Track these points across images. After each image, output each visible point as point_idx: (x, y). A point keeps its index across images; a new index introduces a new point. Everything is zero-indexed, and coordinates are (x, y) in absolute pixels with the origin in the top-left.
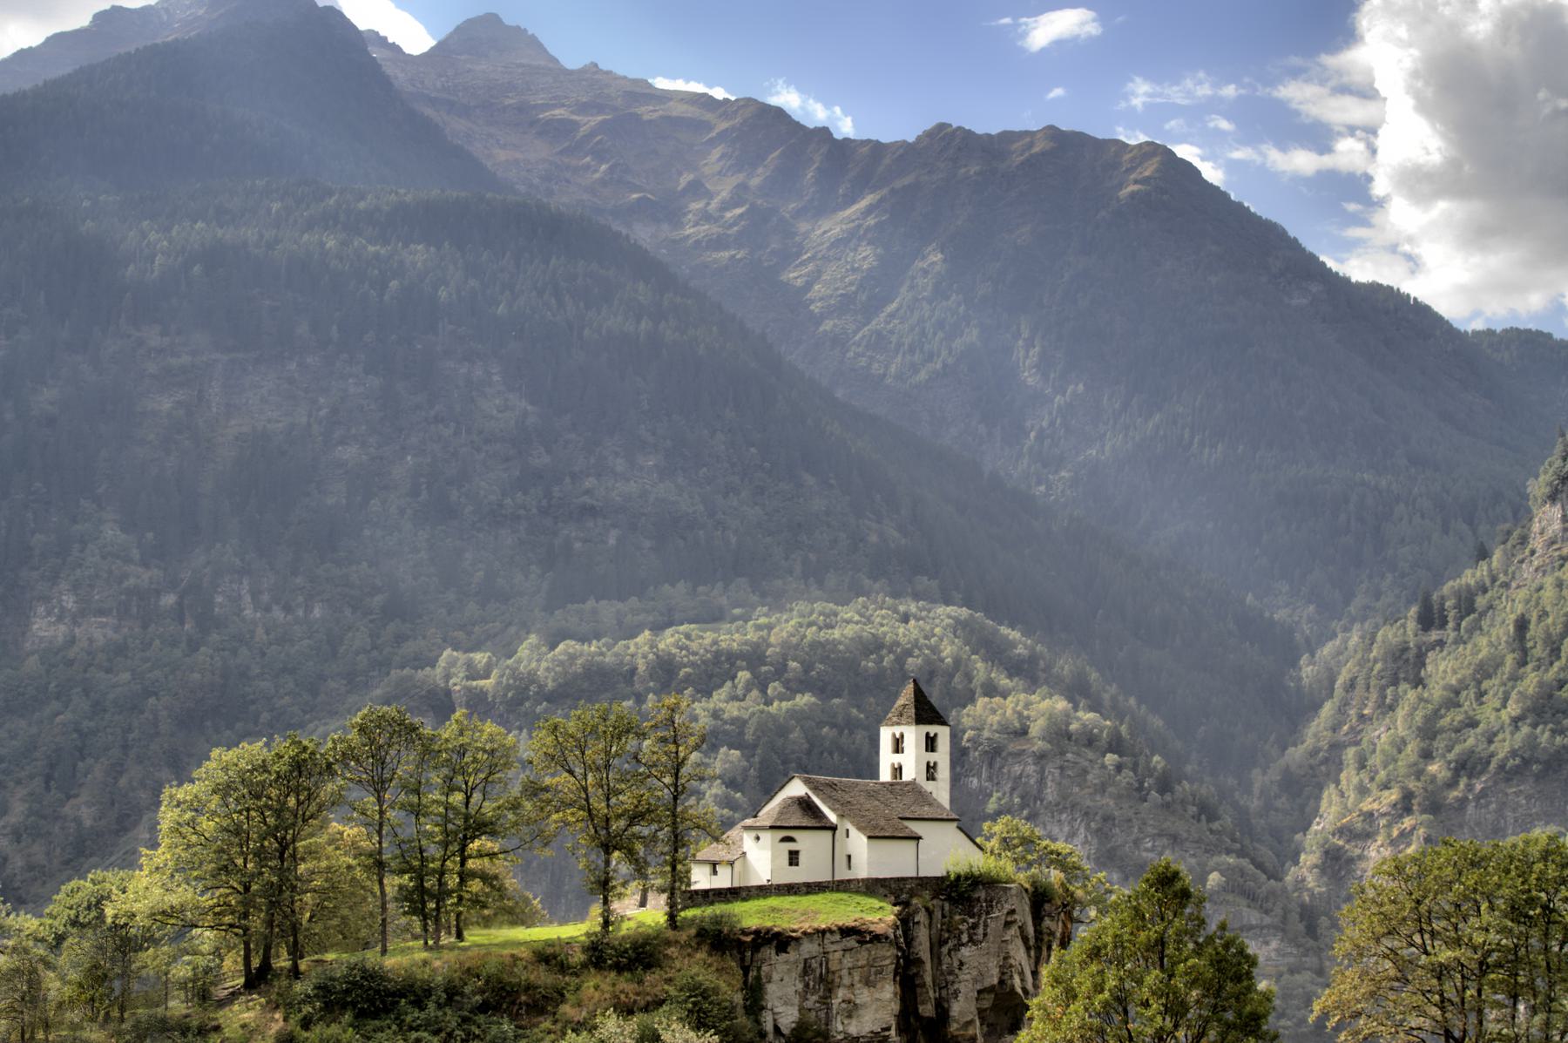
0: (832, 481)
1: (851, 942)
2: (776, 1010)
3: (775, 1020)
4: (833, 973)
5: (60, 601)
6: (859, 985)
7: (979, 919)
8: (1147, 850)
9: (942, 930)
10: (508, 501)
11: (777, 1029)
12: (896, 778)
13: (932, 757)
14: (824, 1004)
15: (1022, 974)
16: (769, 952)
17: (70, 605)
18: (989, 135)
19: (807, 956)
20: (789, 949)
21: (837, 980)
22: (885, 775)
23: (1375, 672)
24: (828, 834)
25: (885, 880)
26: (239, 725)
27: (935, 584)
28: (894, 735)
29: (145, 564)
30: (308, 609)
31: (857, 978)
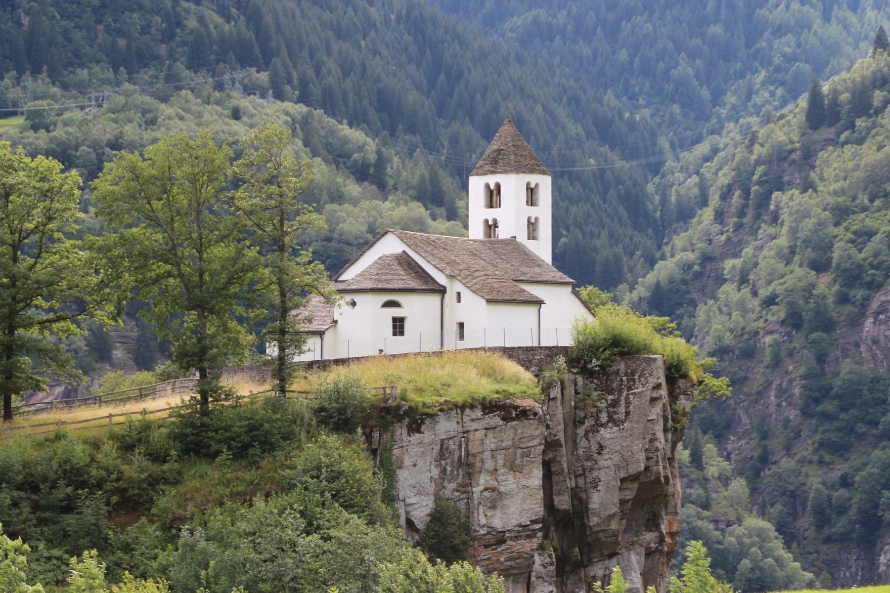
1: (495, 420)
2: (408, 501)
3: (407, 513)
4: (474, 456)
6: (502, 471)
7: (620, 395)
9: (576, 408)
12: (490, 237)
13: (533, 212)
14: (465, 492)
19: (444, 437)
20: (423, 428)
21: (478, 465)
22: (476, 231)
23: (755, 177)
24: (435, 299)
25: (513, 349)
27: (264, 77)
28: (487, 186)
31: (501, 462)
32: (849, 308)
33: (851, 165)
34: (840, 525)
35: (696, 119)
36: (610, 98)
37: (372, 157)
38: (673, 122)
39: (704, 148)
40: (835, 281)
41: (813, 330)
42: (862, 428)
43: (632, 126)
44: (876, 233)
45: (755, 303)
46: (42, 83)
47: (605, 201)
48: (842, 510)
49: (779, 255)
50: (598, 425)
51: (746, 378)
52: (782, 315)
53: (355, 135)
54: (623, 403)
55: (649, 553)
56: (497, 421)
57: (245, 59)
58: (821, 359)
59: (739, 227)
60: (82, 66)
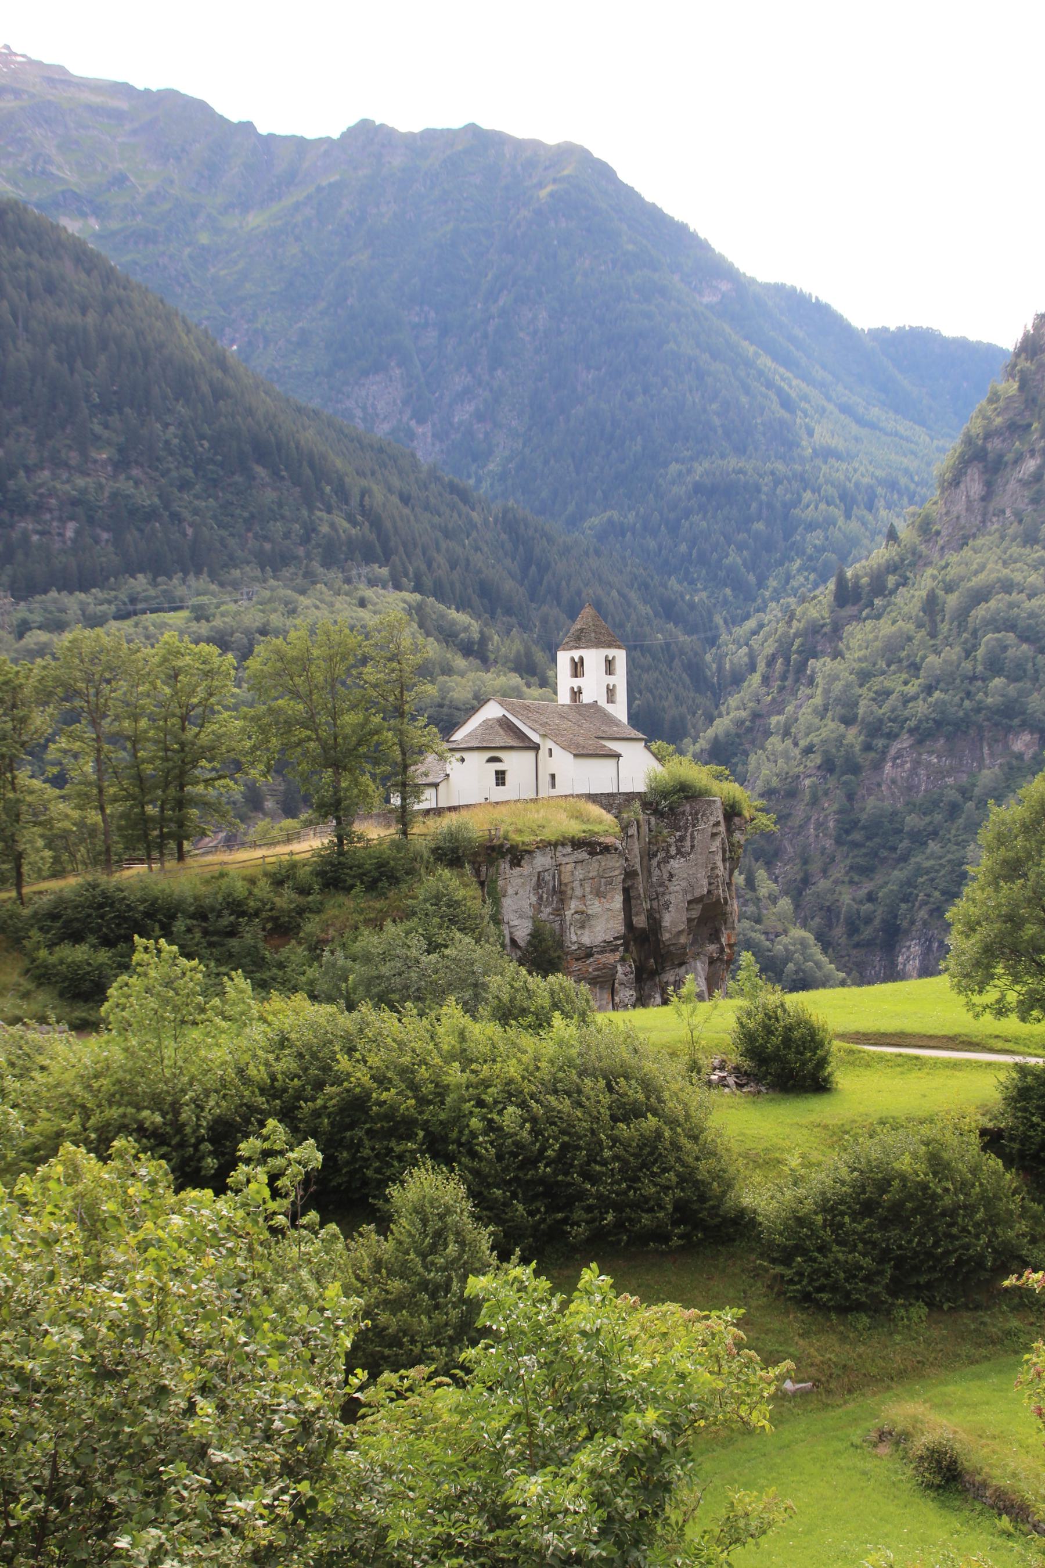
0: (284, 473)
1: (582, 855)
3: (511, 933)
4: (566, 885)
11: (513, 942)
16: (504, 866)
18: (412, 133)
20: (523, 863)
21: (569, 892)
22: (564, 697)
23: (795, 648)
24: (530, 755)
27: (384, 571)
28: (573, 659)
31: (588, 890)
32: (872, 755)
34: (867, 933)
36: (673, 582)
37: (476, 636)
38: (725, 602)
41: (843, 773)
42: (884, 853)
43: (692, 606)
45: (796, 752)
46: (202, 582)
48: (868, 920)
49: (815, 711)
50: (669, 857)
51: (790, 815)
52: (819, 761)
53: (461, 618)
54: (688, 838)
55: (712, 962)
57: (369, 557)
58: (850, 797)
59: (782, 689)
60: (235, 567)
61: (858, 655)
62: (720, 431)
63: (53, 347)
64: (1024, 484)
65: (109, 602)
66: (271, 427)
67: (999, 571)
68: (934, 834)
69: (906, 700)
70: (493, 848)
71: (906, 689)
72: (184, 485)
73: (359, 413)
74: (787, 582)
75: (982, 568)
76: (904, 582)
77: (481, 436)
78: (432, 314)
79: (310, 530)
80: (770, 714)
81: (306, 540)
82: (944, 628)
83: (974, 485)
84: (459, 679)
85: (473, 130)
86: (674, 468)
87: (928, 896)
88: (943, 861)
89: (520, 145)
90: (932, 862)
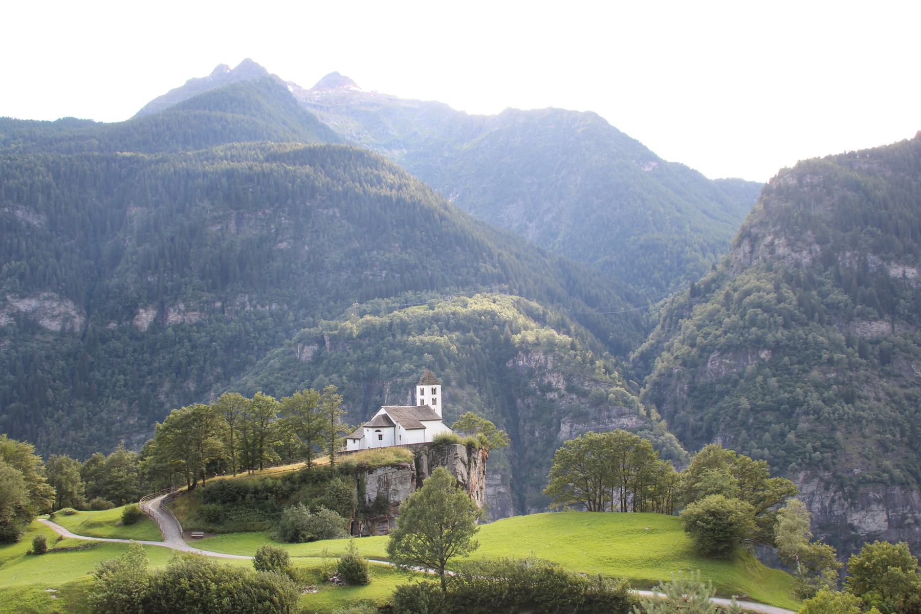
0: (467, 249)
5: (178, 307)
8: (586, 386)
10: (344, 262)
11: (370, 500)
13: (434, 396)
15: (462, 475)
16: (366, 474)
17: (182, 308)
23: (674, 314)
24: (393, 428)
26: (247, 351)
27: (507, 286)
29: (208, 291)
30: (270, 306)
31: (397, 482)
32: (702, 359)
33: (703, 310)
34: (700, 434)
35: (661, 292)
36: (630, 286)
37: (541, 313)
38: (653, 293)
39: (662, 302)
40: (698, 350)
41: (690, 368)
42: (707, 401)
43: (638, 295)
44: (711, 334)
45: (672, 358)
46: (435, 293)
47: (627, 322)
48: (700, 429)
49: (680, 342)
51: (669, 384)
52: (680, 362)
53: (534, 304)
56: (395, 470)
57: (500, 281)
58: (693, 377)
59: (669, 331)
60: (447, 286)
61: (697, 318)
62: (651, 222)
63: (379, 204)
64: (767, 246)
65: (397, 302)
66: (462, 231)
67: (755, 283)
68: (728, 393)
69: (716, 337)
70: (362, 468)
71: (716, 332)
72: (428, 255)
73: (506, 219)
74: (678, 284)
75: (748, 281)
76: (718, 287)
77: (555, 227)
78: (535, 179)
79: (477, 270)
80: (665, 341)
81: (476, 275)
82: (733, 307)
83: (746, 247)
84: (530, 331)
85: (552, 109)
86: (633, 238)
87: (725, 418)
88: (731, 404)
89: (570, 113)
90: (726, 405)
